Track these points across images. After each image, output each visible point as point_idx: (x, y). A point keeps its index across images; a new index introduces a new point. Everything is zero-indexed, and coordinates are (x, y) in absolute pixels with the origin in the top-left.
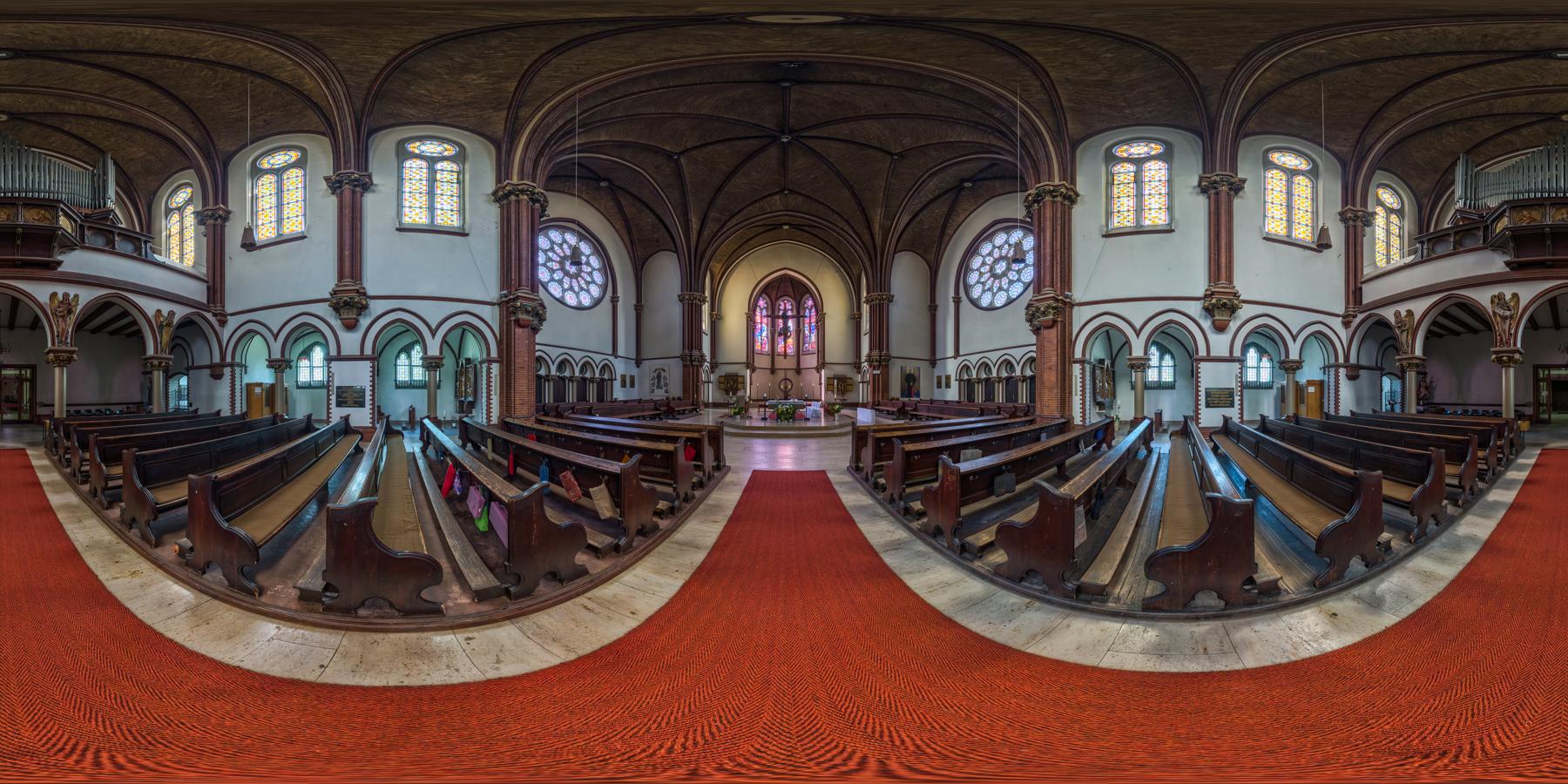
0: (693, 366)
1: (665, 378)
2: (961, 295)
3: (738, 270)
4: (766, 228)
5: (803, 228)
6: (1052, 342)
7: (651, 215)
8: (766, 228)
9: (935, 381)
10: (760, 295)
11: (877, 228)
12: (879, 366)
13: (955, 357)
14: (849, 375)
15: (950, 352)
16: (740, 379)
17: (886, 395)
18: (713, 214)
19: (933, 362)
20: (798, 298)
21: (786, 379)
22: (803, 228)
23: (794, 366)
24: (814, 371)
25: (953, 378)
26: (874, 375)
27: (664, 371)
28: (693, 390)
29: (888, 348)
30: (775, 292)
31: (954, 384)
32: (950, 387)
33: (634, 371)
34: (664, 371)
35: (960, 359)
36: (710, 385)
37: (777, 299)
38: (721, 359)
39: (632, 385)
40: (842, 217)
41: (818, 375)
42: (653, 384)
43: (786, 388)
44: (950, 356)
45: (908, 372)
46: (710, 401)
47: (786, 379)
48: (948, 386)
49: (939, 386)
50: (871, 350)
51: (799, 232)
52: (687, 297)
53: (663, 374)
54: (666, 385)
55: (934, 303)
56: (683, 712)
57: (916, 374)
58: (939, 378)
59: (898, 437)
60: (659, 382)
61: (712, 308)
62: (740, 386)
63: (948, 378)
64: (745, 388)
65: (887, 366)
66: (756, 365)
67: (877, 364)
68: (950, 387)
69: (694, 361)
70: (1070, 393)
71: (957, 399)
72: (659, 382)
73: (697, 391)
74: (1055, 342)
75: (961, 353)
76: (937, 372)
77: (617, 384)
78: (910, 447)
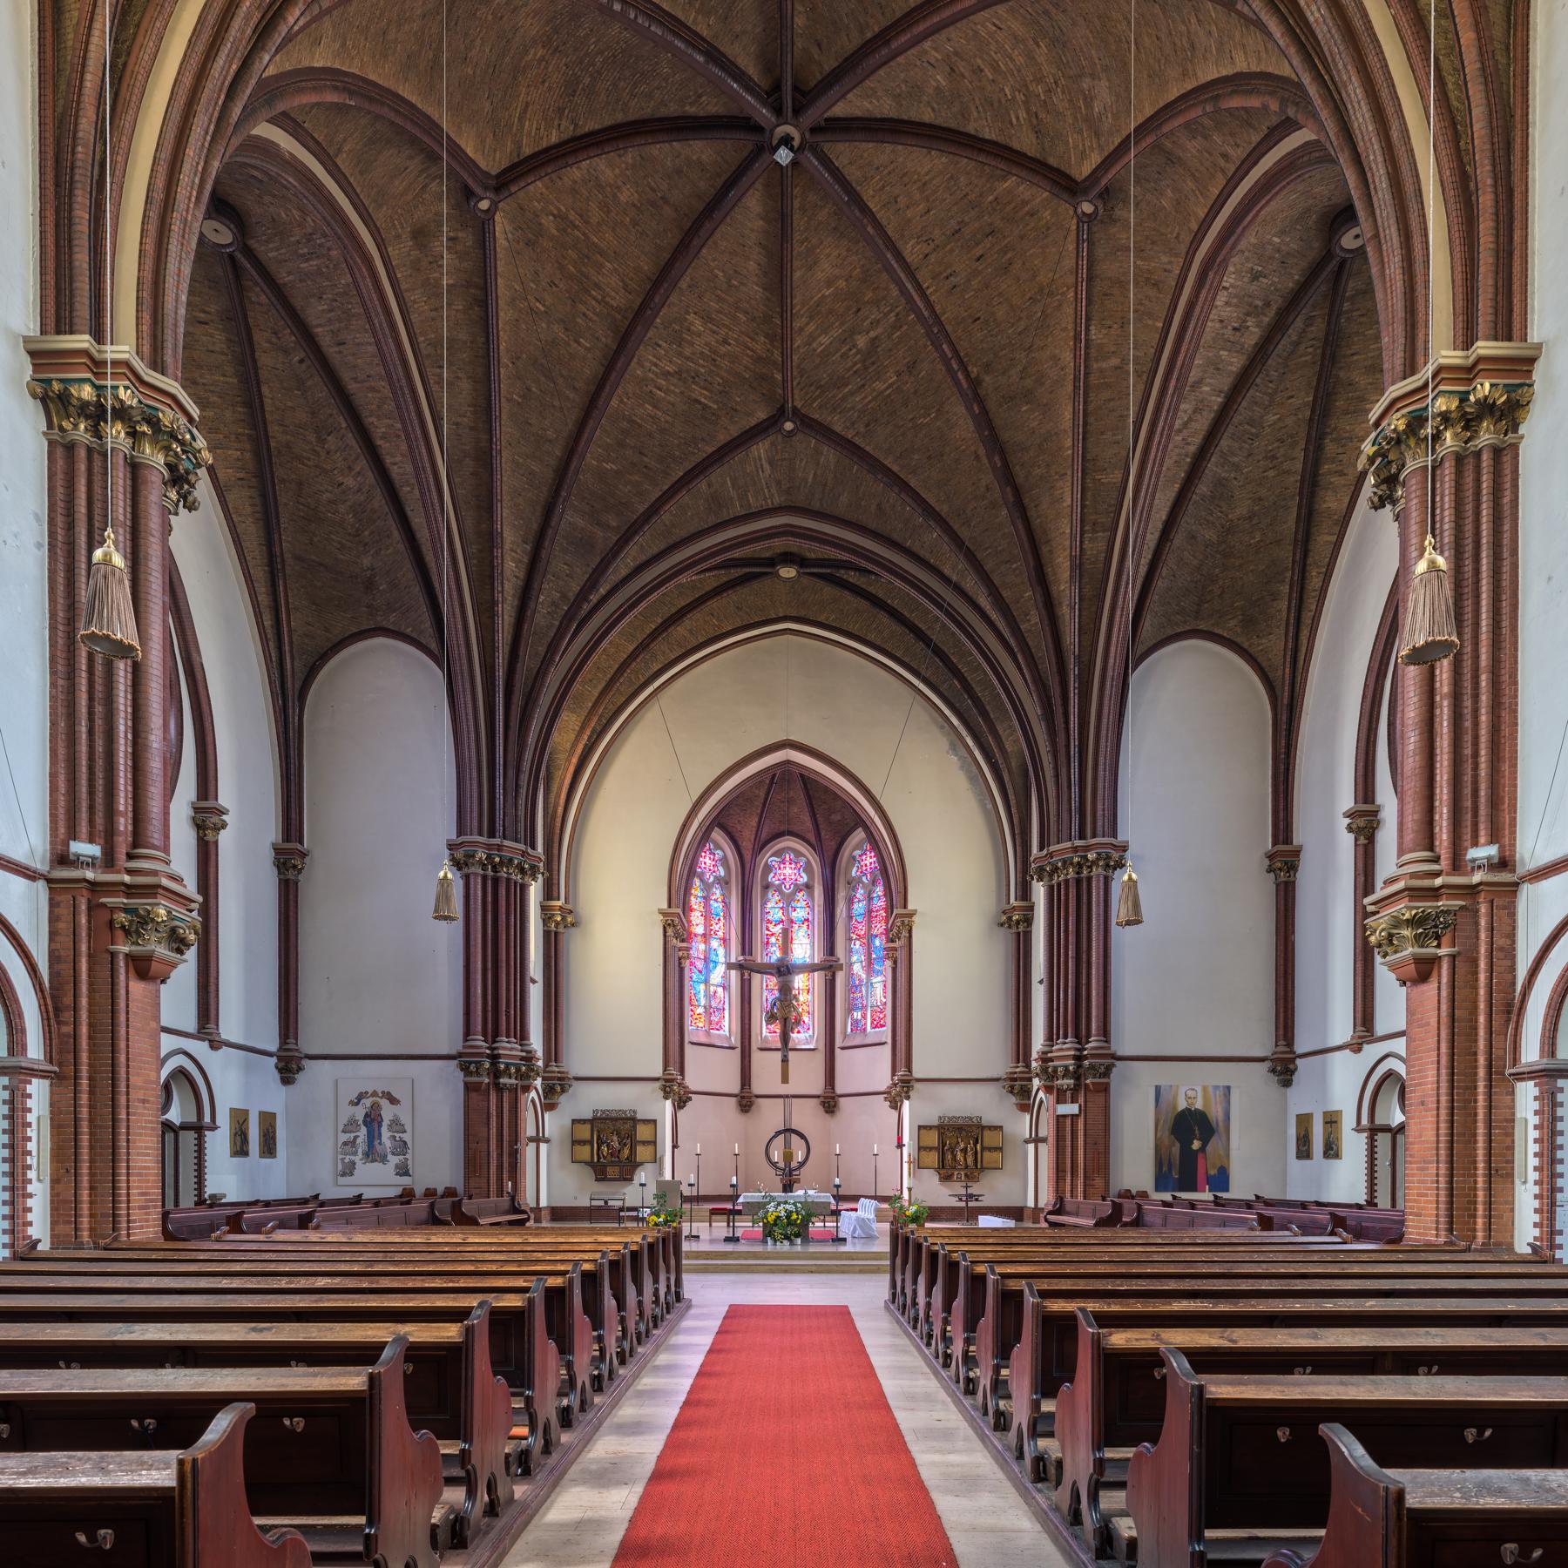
0: (499, 1089)
1: (396, 1125)
2: (1379, 799)
3: (652, 714)
4: (736, 573)
5: (842, 573)
6: (1428, 1024)
7: (362, 464)
8: (736, 573)
9: (1292, 1132)
10: (704, 838)
11: (1065, 574)
12: (1075, 1090)
13: (1356, 1047)
14: (989, 1118)
15: (1341, 1027)
16: (643, 1132)
17: (1099, 1182)
18: (571, 518)
19: (1284, 1068)
20: (830, 845)
21: (788, 1131)
22: (842, 573)
23: (817, 1087)
24: (881, 1104)
25: (1348, 1121)
26: (1060, 1119)
27: (393, 1101)
28: (500, 1167)
29: (1105, 1032)
30: (754, 822)
31: (1354, 1145)
32: (1337, 1156)
33: (272, 1096)
34: (393, 1101)
35: (1373, 1051)
36: (543, 1146)
37: (760, 846)
38: (577, 1061)
39: (269, 1148)
40: (958, 542)
41: (895, 1114)
42: (352, 1143)
43: (788, 1157)
44: (1338, 1042)
45: (1182, 1105)
46: (543, 1203)
47: (788, 1131)
48: (1332, 1150)
49: (1304, 1152)
50: (1050, 1038)
51: (828, 591)
52: (481, 855)
53: (388, 1112)
54: (401, 1148)
55: (1288, 840)
56: (576, 227)
57: (1215, 1113)
58: (1304, 1121)
59: (1359, 1418)
60: (373, 1136)
61: (549, 892)
62: (642, 1152)
63: (1332, 1120)
64: (656, 1160)
65: (1105, 1089)
66: (693, 1080)
67: (1068, 1082)
68: (1337, 1156)
69: (507, 1073)
70: (1509, 1176)
71: (1361, 1198)
72: (373, 1136)
73: (514, 1168)
74: (1434, 1021)
75: (1381, 1028)
76: (1300, 1099)
77: (218, 1143)
78: (1224, 1388)
